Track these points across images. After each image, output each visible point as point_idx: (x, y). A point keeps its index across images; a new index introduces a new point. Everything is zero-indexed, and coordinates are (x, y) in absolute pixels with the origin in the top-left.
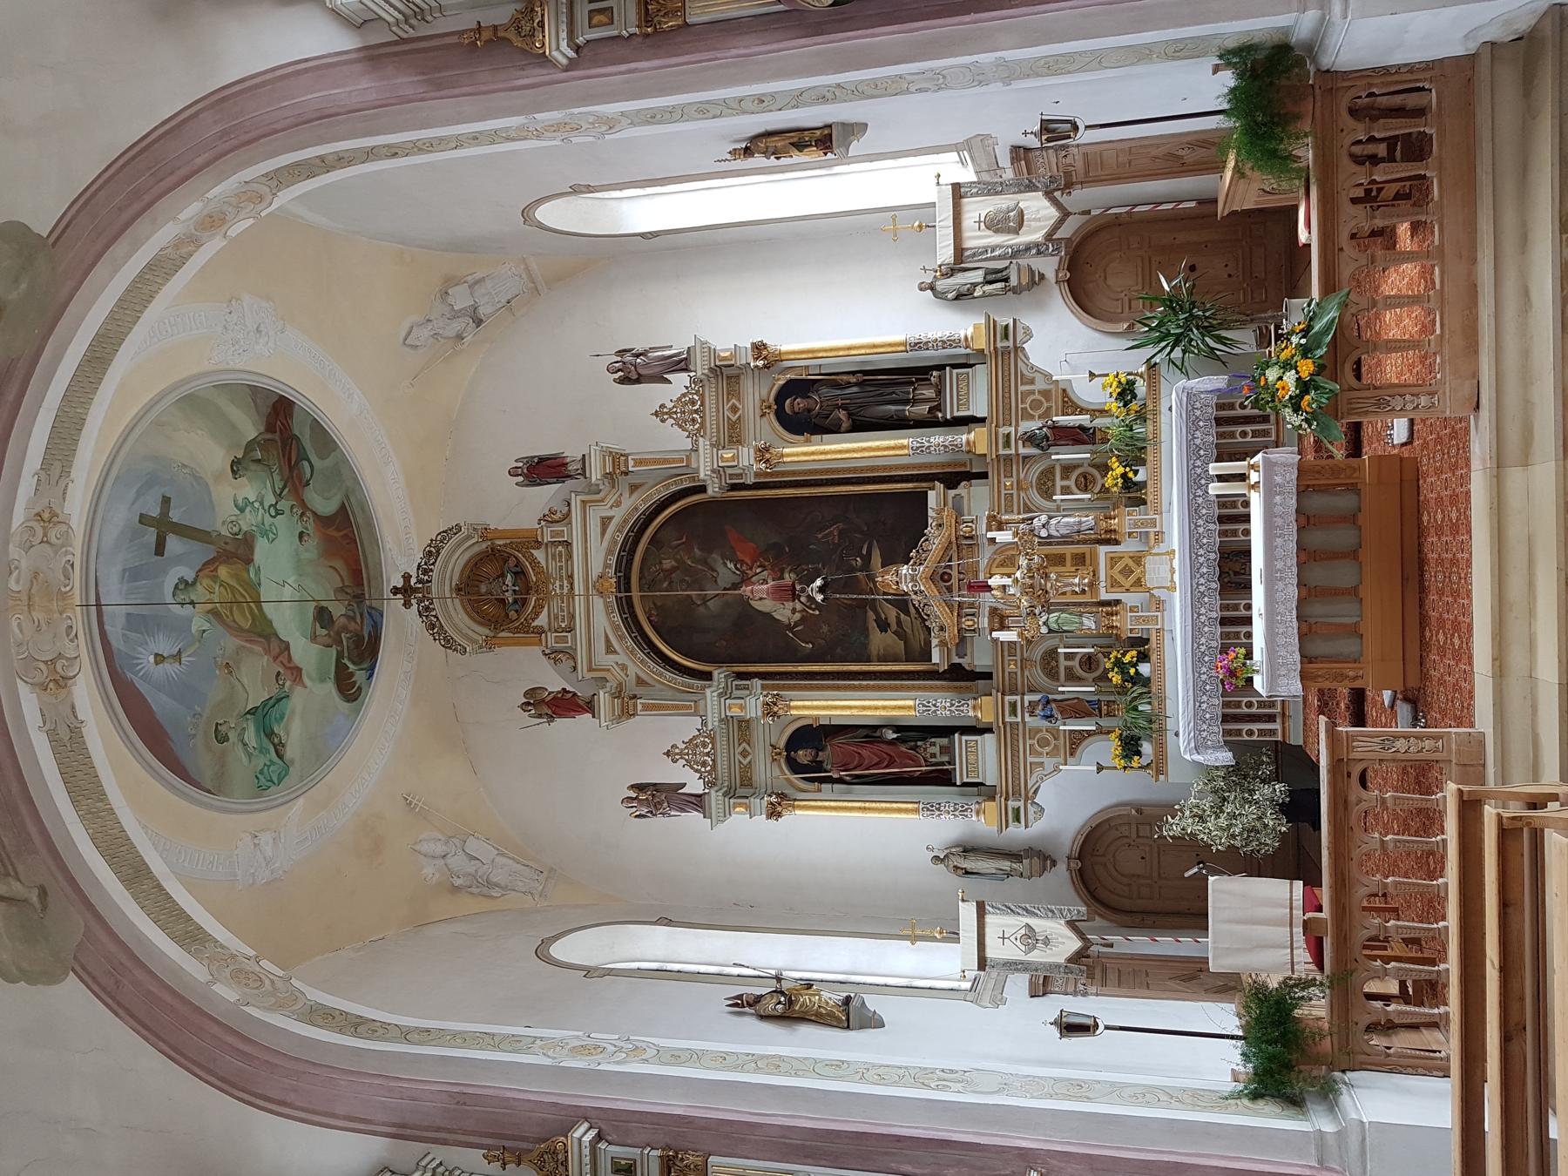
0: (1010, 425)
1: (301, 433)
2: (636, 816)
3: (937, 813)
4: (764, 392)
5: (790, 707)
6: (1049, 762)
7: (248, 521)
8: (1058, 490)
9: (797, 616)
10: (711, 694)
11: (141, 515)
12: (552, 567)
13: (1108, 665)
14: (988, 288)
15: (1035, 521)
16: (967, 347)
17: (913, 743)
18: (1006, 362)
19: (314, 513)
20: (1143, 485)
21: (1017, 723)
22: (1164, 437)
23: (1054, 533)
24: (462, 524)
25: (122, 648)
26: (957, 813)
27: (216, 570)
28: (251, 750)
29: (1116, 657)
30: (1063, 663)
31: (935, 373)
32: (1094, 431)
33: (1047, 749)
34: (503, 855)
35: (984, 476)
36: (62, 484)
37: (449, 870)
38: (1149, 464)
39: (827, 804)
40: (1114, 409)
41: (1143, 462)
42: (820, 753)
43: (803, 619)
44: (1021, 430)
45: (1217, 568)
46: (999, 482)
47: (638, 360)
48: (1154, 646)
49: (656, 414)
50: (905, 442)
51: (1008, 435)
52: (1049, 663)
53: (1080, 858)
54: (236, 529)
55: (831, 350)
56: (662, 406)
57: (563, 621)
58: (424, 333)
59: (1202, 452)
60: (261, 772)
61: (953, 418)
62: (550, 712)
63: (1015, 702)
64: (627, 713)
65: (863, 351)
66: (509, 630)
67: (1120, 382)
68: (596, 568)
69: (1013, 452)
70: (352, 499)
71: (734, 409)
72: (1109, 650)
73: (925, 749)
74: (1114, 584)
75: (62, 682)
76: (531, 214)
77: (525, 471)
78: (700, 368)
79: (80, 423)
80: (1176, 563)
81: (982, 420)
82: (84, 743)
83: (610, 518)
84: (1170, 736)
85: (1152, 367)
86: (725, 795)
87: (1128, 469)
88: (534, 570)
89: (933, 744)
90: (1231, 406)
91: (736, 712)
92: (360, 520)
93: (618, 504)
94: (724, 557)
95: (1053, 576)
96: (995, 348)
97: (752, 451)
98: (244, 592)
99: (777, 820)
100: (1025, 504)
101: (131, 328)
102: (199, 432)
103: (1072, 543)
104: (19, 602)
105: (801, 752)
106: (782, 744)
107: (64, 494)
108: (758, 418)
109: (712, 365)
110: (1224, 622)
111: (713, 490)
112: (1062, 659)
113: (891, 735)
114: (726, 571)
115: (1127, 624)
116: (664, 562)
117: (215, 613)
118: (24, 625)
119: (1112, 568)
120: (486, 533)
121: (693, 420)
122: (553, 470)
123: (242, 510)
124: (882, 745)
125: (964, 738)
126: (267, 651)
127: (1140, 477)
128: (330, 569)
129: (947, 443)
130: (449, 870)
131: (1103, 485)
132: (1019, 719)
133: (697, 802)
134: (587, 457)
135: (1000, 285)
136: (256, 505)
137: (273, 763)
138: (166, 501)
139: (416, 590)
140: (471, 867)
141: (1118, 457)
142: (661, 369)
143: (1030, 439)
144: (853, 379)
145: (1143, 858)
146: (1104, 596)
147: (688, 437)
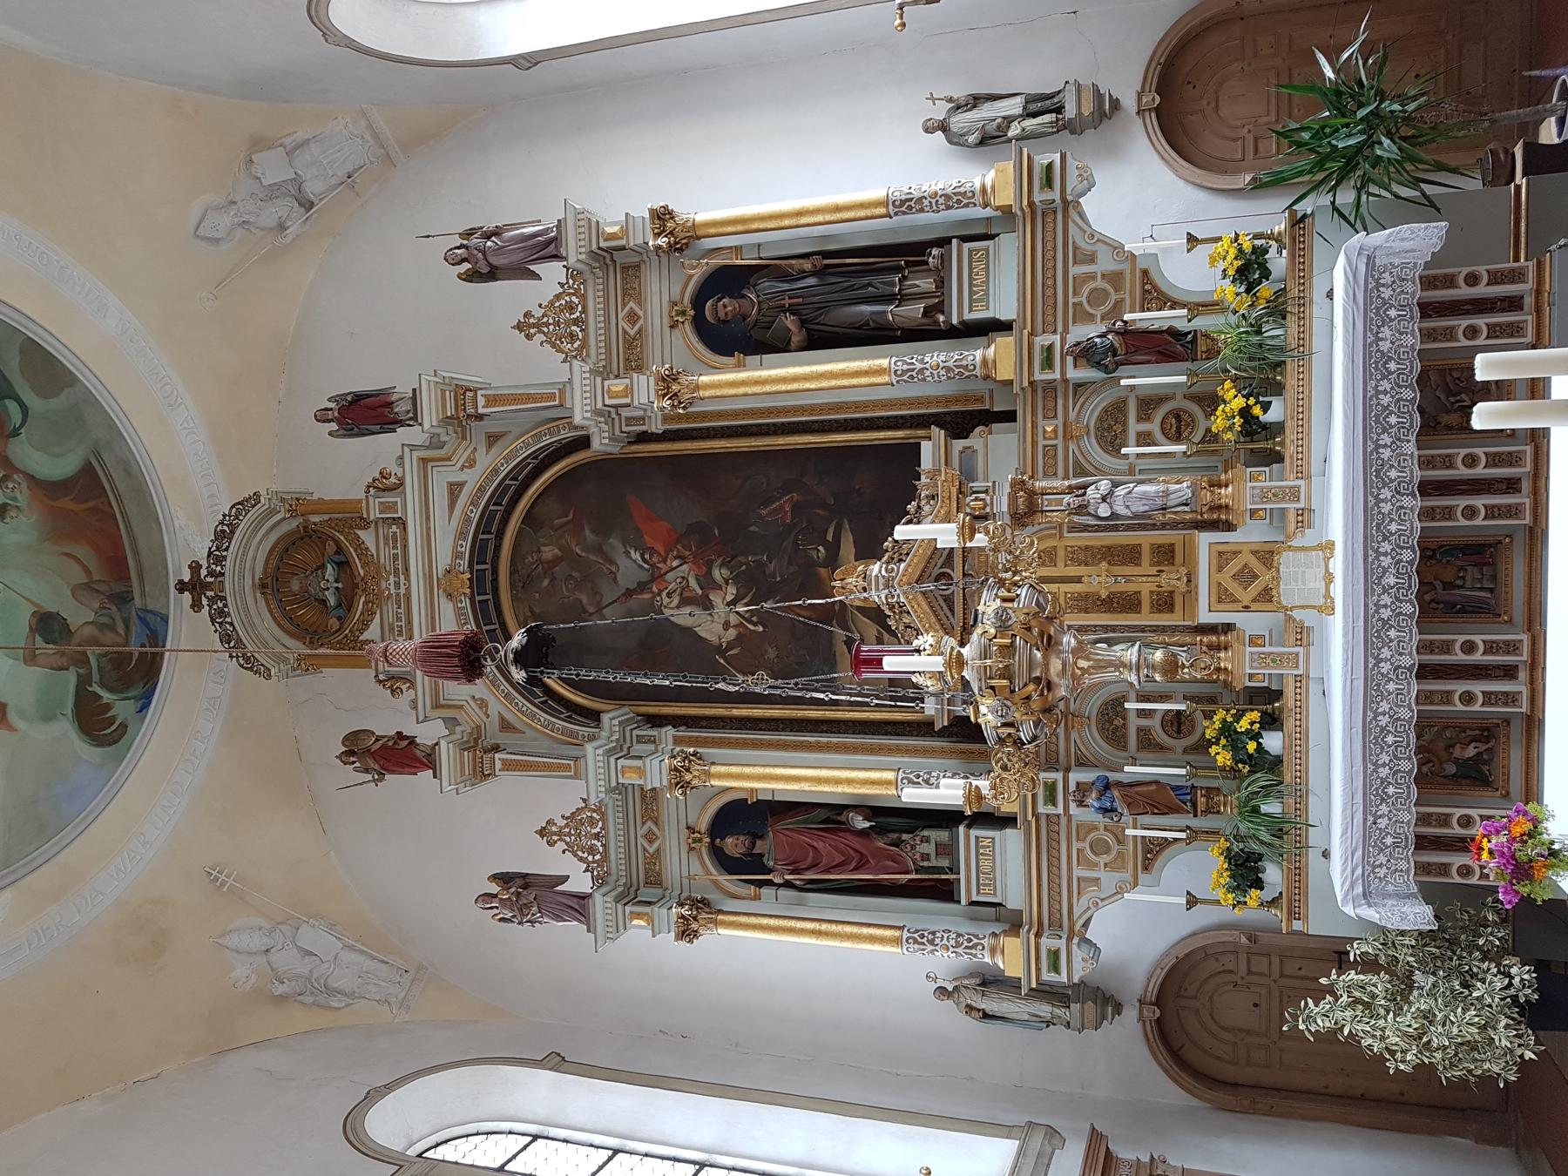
0: (1055, 416)
2: (501, 920)
3: (930, 948)
4: (676, 290)
5: (709, 775)
6: (1109, 879)
8: (1132, 437)
9: (732, 633)
10: (593, 753)
12: (384, 556)
13: (1209, 734)
14: (1030, 123)
15: (1090, 490)
16: (986, 205)
17: (895, 836)
18: (1049, 227)
19: (32, 479)
20: (1279, 428)
21: (1058, 816)
22: (1317, 344)
23: (1121, 510)
26: (960, 950)
29: (1224, 720)
30: (1134, 723)
31: (935, 251)
32: (1195, 337)
33: (1105, 858)
34: (351, 948)
35: (1010, 416)
38: (1289, 392)
39: (765, 921)
40: (1230, 298)
41: (1278, 389)
42: (759, 843)
43: (739, 637)
44: (1072, 339)
45: (1415, 578)
46: (1034, 425)
48: (1291, 703)
49: (519, 327)
50: (884, 362)
51: (1050, 349)
52: (1111, 722)
53: (1158, 1003)
55: (771, 217)
56: (527, 315)
58: (226, 220)
59: (1392, 366)
61: (963, 322)
62: (377, 767)
63: (1054, 784)
64: (481, 774)
65: (820, 218)
66: (331, 646)
67: (1240, 250)
68: (443, 559)
69: (1057, 376)
70: (106, 456)
71: (633, 318)
72: (1212, 707)
73: (913, 847)
74: (1223, 597)
77: (336, 414)
78: (574, 251)
80: (1337, 565)
81: (1004, 327)
83: (461, 485)
84: (1314, 857)
85: (1298, 221)
86: (617, 900)
87: (1252, 401)
88: (360, 560)
89: (926, 840)
90: (1450, 282)
91: (631, 779)
92: (122, 487)
93: (471, 463)
95: (1069, 641)
96: (1031, 204)
97: (652, 380)
99: (691, 941)
100: (1077, 463)
103: (1154, 527)
105: (729, 840)
106: (704, 824)
108: (667, 330)
109: (594, 247)
110: (1425, 672)
111: (601, 443)
112: (1132, 717)
113: (861, 823)
114: (629, 565)
115: (1244, 666)
116: (543, 549)
119: (1220, 569)
120: (298, 505)
121: (572, 336)
122: (373, 413)
124: (848, 835)
125: (974, 833)
127: (1274, 415)
128: (65, 558)
129: (950, 364)
130: (272, 970)
131: (1208, 430)
132: (1060, 810)
133: (578, 907)
134: (418, 391)
135: (1047, 118)
139: (208, 586)
140: (302, 966)
141: (1235, 380)
143: (1086, 353)
144: (807, 265)
145: (1256, 1005)
146: (1205, 617)
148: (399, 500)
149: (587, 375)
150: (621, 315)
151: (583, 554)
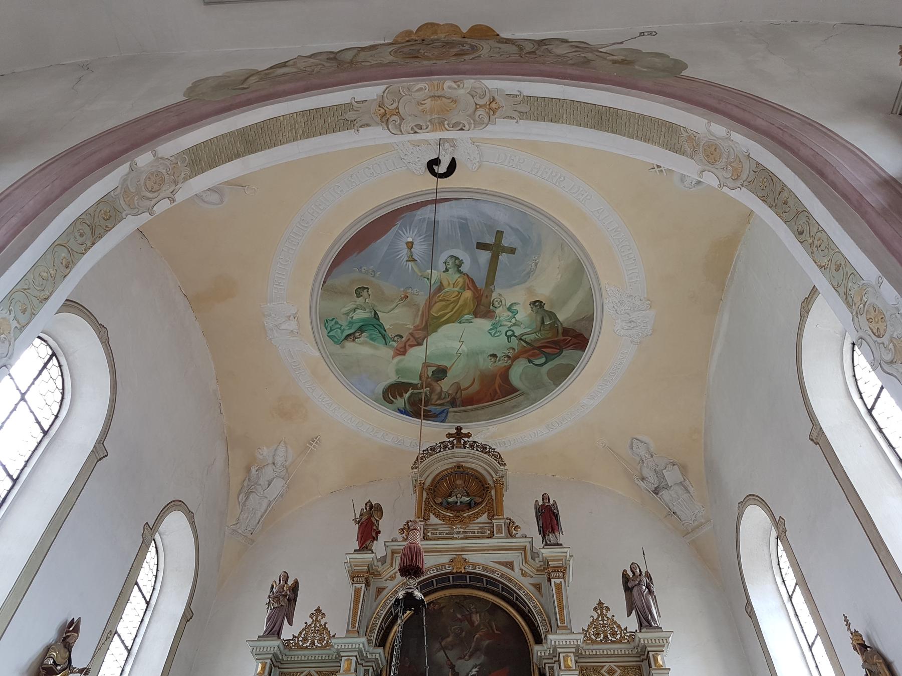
1: (564, 356)
2: (273, 586)
7: (502, 313)
11: (502, 232)
12: (474, 527)
19: (509, 367)
24: (506, 468)
25: (417, 218)
27: (469, 289)
28: (351, 315)
34: (269, 505)
36: (515, 115)
37: (264, 466)
47: (644, 587)
54: (496, 304)
56: (608, 609)
57: (432, 534)
58: (643, 452)
60: (337, 323)
64: (354, 576)
68: (472, 558)
75: (384, 119)
76: (750, 502)
77: (547, 504)
78: (645, 636)
79: (556, 119)
82: (344, 130)
83: (512, 569)
88: (472, 514)
91: (344, 665)
92: (507, 404)
93: (524, 574)
94: (481, 665)
98: (454, 310)
101: (624, 136)
102: (559, 276)
104: (436, 89)
107: (508, 117)
109: (649, 649)
117: (441, 288)
118: (421, 93)
120: (500, 484)
121: (598, 635)
123: (509, 309)
126: (417, 328)
130: (264, 466)
133: (274, 630)
136: (513, 320)
137: (342, 331)
138: (512, 251)
139: (459, 441)
140: (263, 481)
142: (640, 606)
147: (583, 630)
148: (503, 535)
149: (576, 643)
150: (612, 664)
151: (475, 639)
